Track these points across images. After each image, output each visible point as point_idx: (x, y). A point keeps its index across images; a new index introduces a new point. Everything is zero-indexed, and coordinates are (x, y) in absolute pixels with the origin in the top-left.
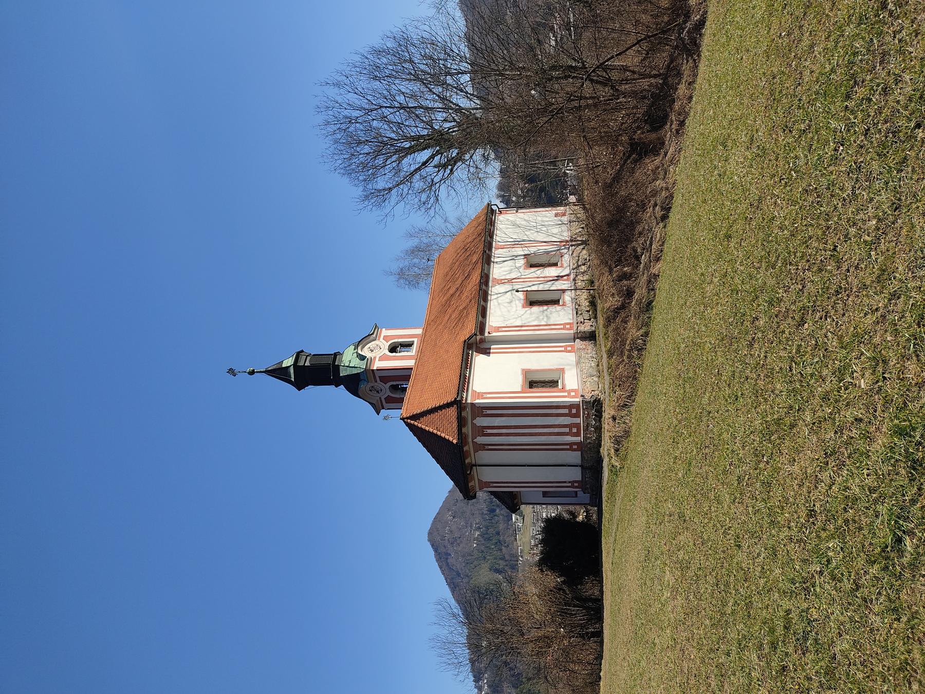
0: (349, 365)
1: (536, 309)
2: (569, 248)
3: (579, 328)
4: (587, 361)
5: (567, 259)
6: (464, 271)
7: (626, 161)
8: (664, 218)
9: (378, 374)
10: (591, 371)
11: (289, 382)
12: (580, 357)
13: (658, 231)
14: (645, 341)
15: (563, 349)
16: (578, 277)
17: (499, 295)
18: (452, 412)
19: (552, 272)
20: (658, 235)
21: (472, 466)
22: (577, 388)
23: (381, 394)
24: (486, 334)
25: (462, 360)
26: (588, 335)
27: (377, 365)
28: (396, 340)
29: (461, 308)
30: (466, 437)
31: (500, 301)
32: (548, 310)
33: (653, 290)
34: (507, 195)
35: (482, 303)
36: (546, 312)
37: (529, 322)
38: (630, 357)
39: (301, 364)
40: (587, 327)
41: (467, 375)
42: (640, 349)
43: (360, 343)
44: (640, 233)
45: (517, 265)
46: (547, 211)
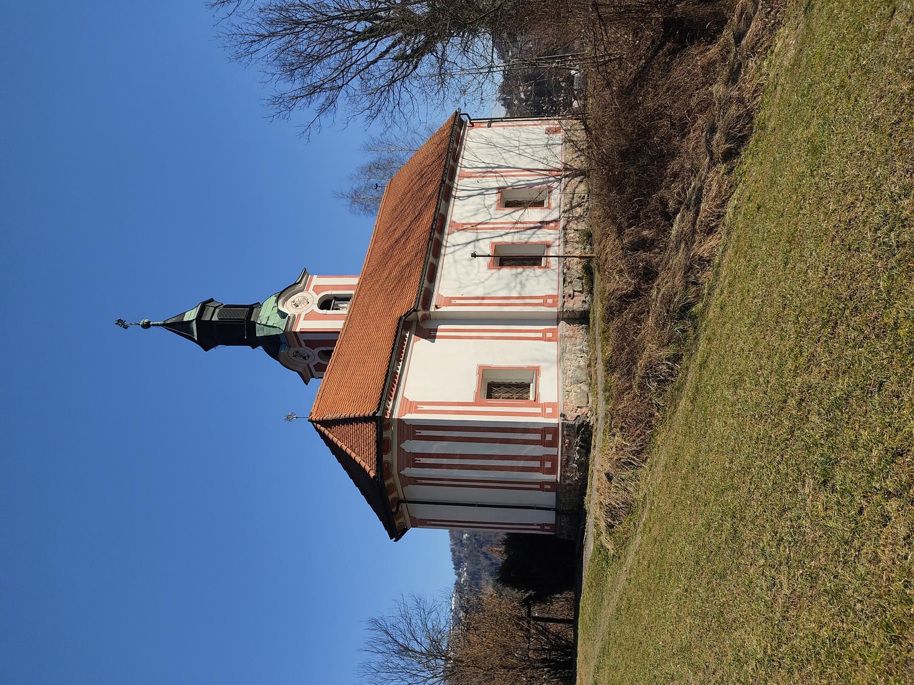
0: (267, 323)
1: (506, 272)
2: (561, 180)
3: (566, 304)
4: (573, 356)
5: (556, 198)
6: (415, 207)
7: (656, 52)
8: (729, 155)
10: (579, 375)
11: (193, 340)
12: (563, 351)
13: (715, 179)
14: (672, 369)
15: (540, 335)
16: (571, 224)
17: (457, 247)
18: (369, 430)
19: (534, 215)
20: (715, 187)
21: (400, 502)
22: (557, 401)
24: (432, 309)
25: (393, 349)
26: (578, 315)
27: (302, 325)
29: (404, 263)
30: (389, 465)
31: (457, 257)
32: (524, 274)
33: (694, 283)
34: (509, 98)
35: (431, 259)
36: (520, 277)
37: (494, 292)
38: (642, 387)
39: (207, 318)
40: (577, 304)
41: (399, 372)
42: (661, 381)
43: (282, 295)
44: (675, 175)
45: (487, 203)
46: (536, 125)
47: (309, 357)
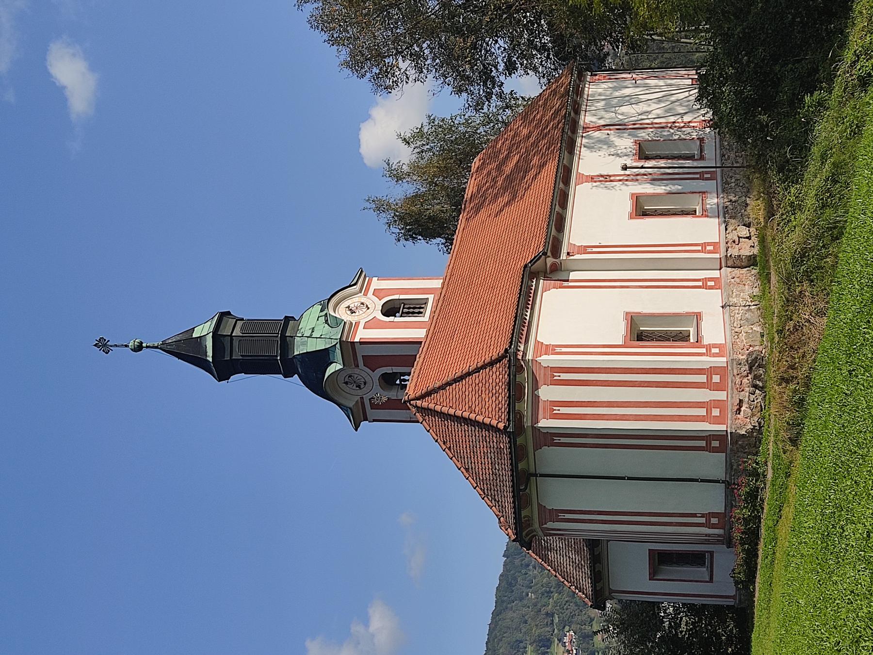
9: (361, 352)
18: (498, 375)
23: (365, 390)
24: (563, 256)
25: (520, 294)
27: (362, 335)
28: (396, 297)
41: (528, 318)
47: (365, 383)
